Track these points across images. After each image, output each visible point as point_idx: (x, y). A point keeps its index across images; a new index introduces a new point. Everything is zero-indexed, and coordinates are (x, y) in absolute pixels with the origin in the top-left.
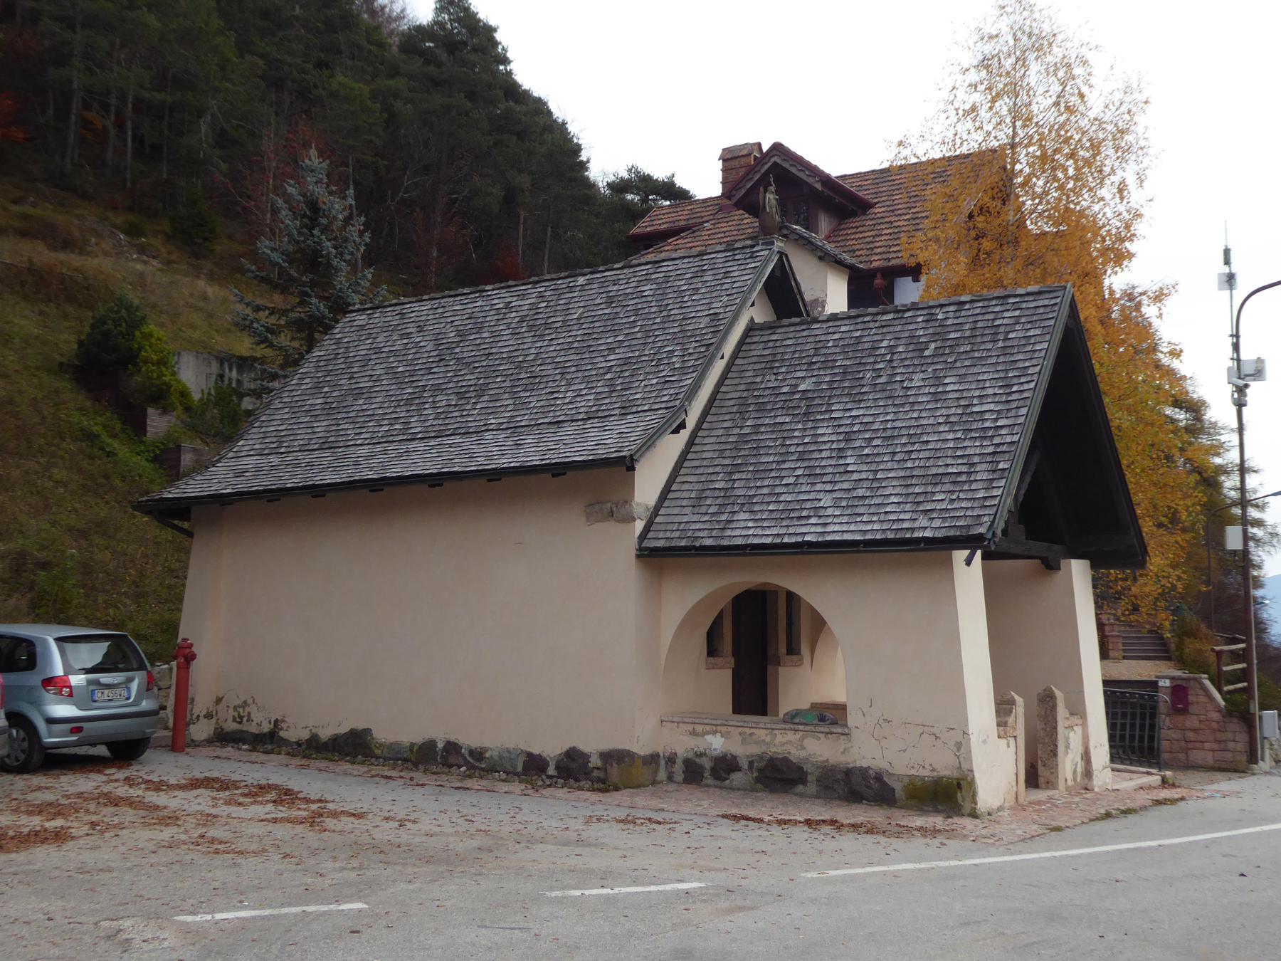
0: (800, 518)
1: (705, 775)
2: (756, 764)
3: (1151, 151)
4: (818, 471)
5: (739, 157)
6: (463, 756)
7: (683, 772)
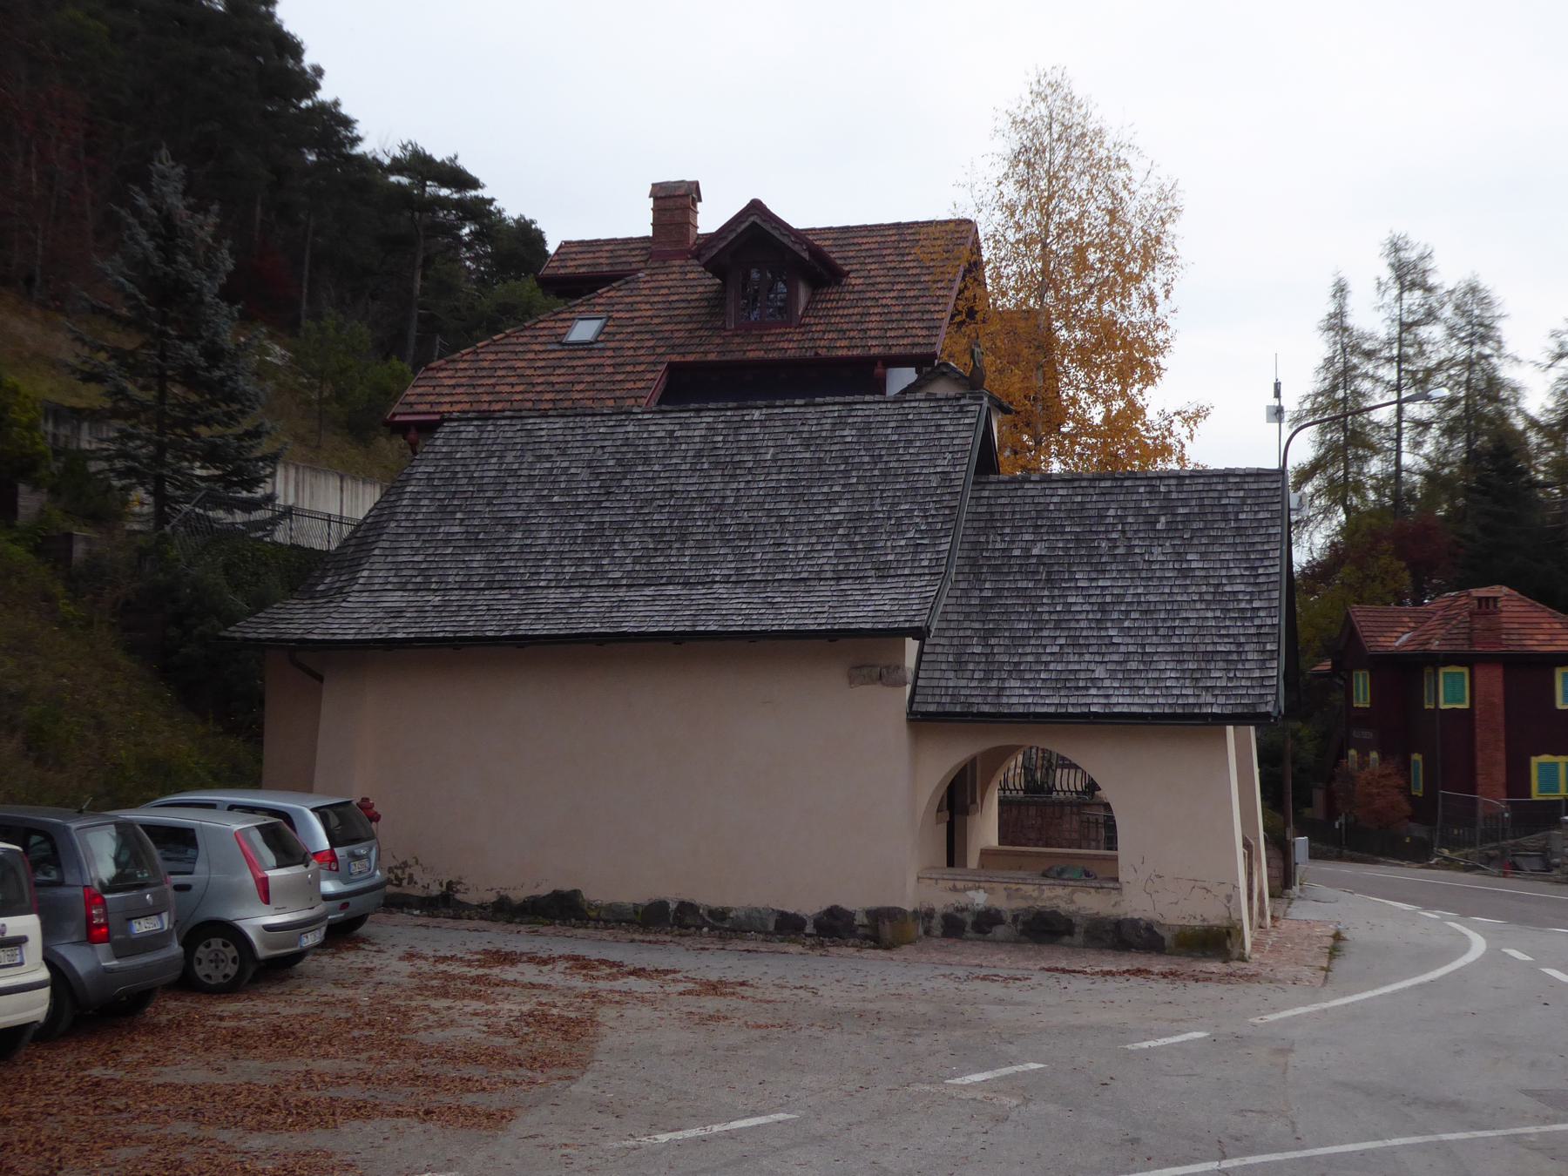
0: (1078, 688)
1: (967, 929)
2: (1021, 917)
3: (1178, 262)
4: (1081, 642)
5: (675, 196)
6: (701, 916)
7: (942, 927)
